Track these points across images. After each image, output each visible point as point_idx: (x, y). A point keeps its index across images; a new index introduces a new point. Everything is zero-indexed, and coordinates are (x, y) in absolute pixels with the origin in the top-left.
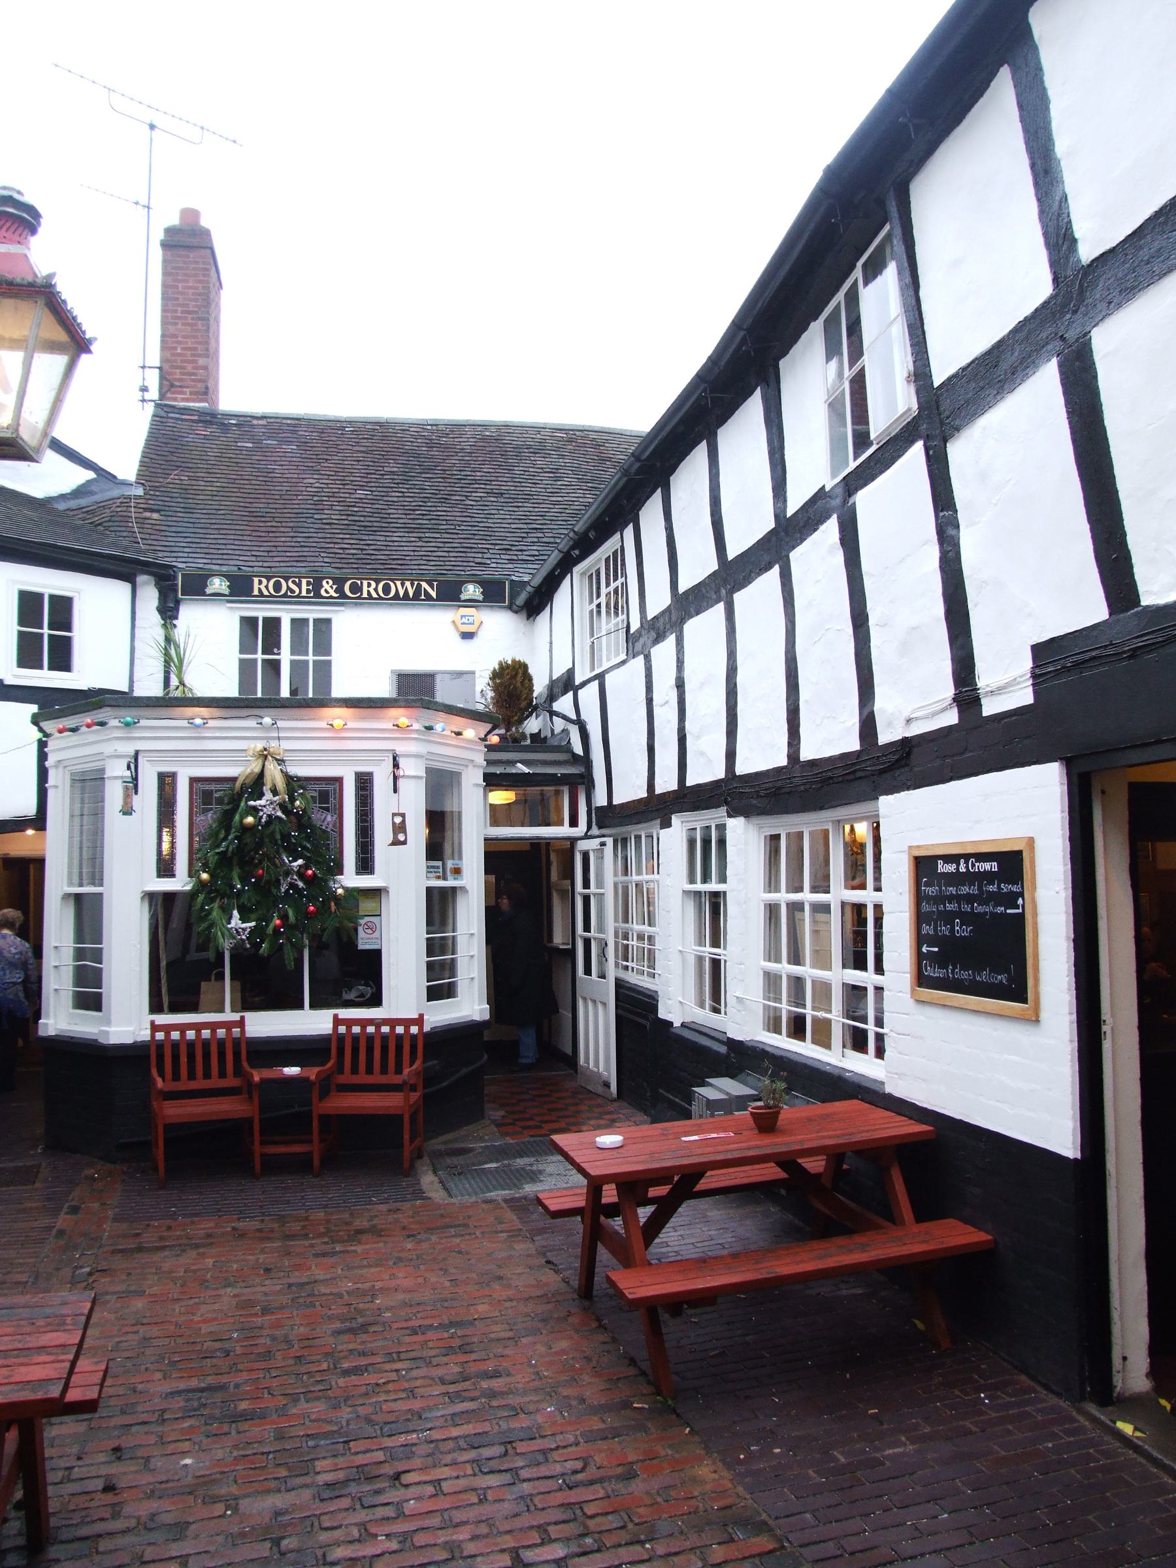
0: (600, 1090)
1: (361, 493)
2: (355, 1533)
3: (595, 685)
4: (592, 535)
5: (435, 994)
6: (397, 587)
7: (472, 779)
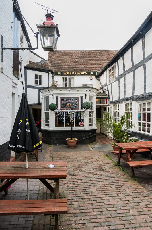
0: (110, 138)
1: (76, 61)
2: (67, 186)
3: (110, 85)
4: (110, 64)
5: (90, 125)
6: (82, 73)
7: (95, 97)
